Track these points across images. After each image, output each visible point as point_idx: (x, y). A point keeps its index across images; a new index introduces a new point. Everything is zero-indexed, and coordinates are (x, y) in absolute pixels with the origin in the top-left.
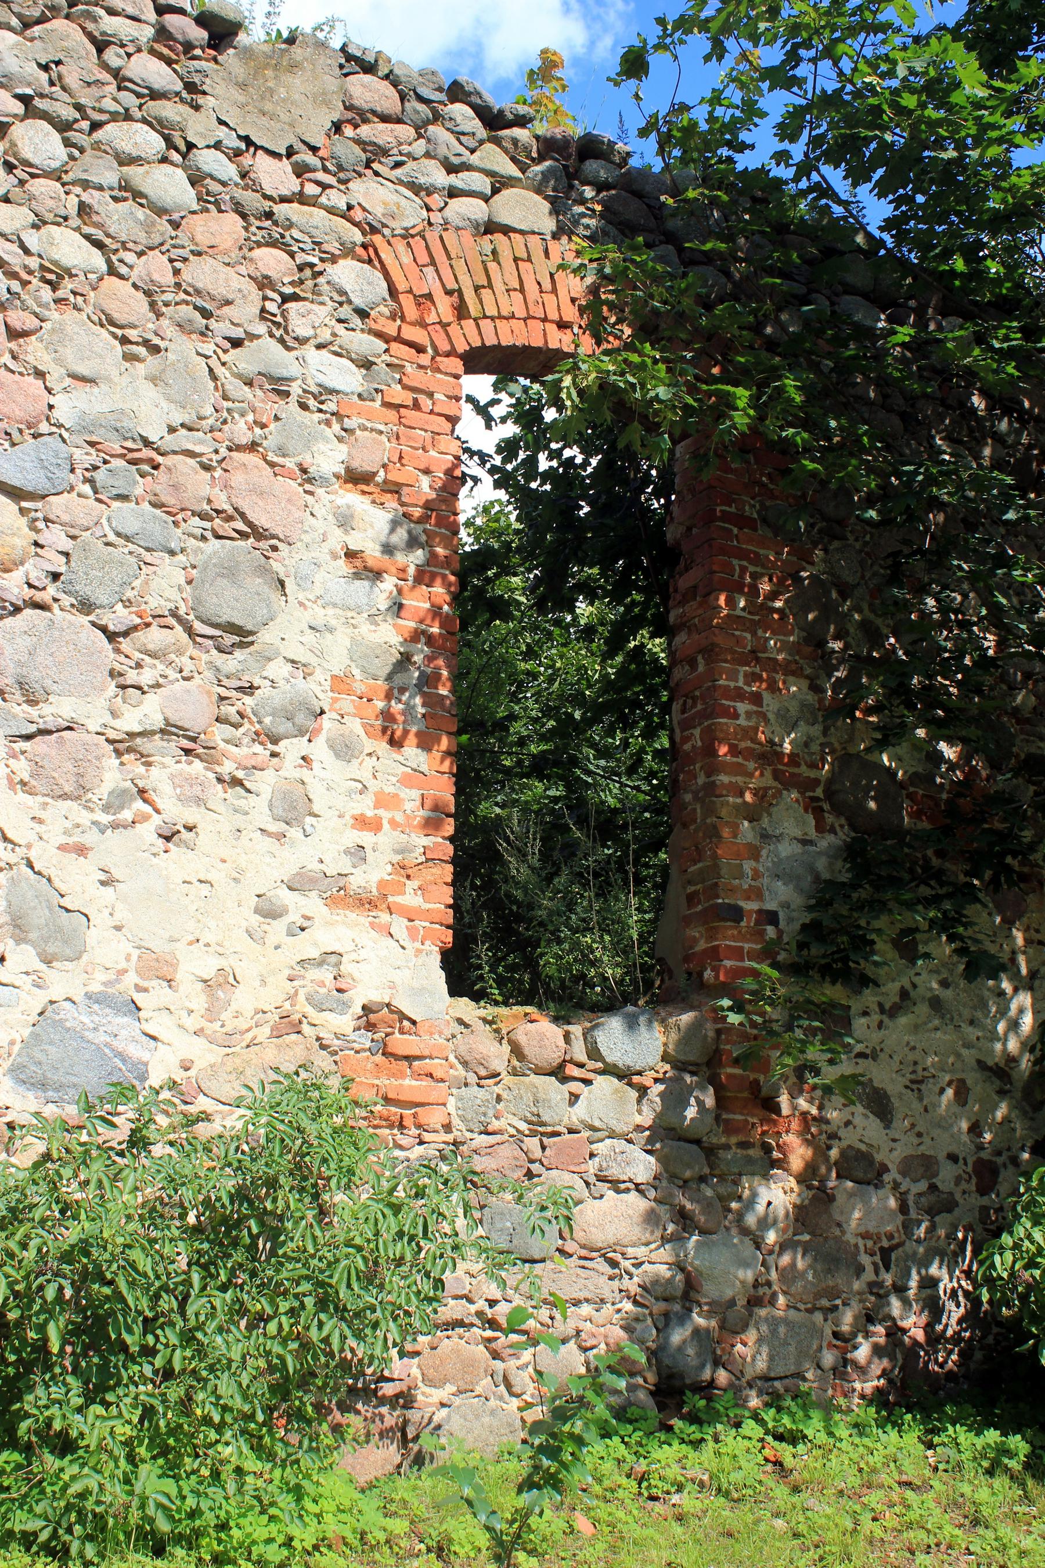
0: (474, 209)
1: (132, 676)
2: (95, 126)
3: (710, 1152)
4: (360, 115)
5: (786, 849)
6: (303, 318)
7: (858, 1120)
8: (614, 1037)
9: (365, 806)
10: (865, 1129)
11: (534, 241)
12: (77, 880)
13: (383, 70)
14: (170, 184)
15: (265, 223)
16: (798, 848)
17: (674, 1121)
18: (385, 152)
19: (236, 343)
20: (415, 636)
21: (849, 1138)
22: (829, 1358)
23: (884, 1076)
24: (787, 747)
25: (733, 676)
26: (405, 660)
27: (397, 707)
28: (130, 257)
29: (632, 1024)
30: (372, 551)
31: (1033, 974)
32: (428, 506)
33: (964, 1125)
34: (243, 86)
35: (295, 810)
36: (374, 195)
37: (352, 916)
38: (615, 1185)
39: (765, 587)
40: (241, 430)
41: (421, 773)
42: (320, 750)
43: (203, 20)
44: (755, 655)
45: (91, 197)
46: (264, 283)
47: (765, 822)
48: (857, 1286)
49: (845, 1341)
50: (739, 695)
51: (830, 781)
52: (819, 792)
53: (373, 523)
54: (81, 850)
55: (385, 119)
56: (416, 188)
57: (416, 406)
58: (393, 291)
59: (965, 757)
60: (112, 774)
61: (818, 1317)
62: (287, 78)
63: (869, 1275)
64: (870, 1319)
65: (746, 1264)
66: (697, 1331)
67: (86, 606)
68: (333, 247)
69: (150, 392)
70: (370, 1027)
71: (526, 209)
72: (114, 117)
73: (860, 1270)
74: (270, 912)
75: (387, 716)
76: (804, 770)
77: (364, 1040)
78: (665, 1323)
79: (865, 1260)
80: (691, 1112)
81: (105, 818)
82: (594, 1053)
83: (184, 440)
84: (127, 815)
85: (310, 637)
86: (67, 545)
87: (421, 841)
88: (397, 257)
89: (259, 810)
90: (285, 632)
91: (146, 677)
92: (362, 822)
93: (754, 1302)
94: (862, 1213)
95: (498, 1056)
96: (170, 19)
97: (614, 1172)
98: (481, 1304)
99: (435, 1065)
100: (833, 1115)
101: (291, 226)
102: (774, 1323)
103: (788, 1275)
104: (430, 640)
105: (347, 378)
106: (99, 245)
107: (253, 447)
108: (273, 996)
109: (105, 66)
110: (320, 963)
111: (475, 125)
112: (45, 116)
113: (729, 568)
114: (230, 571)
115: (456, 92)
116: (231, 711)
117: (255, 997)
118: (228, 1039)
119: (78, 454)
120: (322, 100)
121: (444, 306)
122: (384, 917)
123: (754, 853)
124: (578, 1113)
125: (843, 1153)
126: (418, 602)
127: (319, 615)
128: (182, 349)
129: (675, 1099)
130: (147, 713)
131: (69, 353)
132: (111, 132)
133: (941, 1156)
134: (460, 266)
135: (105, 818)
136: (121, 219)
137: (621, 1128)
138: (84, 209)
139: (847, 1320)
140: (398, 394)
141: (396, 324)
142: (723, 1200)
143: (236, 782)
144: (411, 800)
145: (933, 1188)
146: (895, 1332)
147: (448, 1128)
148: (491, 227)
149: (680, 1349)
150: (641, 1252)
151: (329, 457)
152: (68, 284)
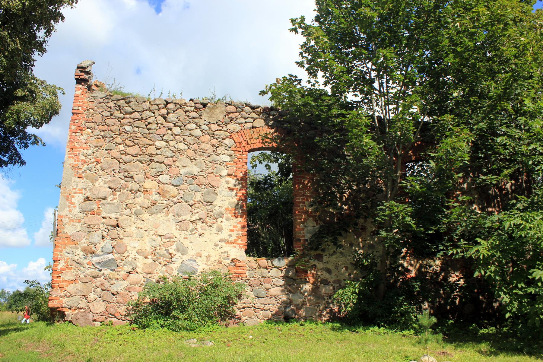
0: (250, 125)
1: (194, 211)
2: (185, 125)
3: (295, 280)
4: (229, 113)
5: (309, 228)
6: (219, 151)
7: (324, 274)
8: (276, 262)
9: (232, 228)
10: (326, 276)
11: (261, 129)
12: (186, 243)
13: (233, 104)
14: (198, 132)
15: (213, 136)
16: (312, 228)
17: (287, 275)
18: (233, 119)
19: (209, 156)
20: (239, 200)
21: (322, 277)
22: (317, 314)
23: (330, 266)
24: (310, 210)
25: (299, 199)
26: (238, 204)
27: (236, 211)
28: (191, 146)
29: (279, 260)
30: (232, 187)
31: (363, 246)
32: (241, 178)
33: (347, 274)
34: (208, 113)
35: (220, 229)
36: (232, 126)
37: (230, 245)
38: (276, 285)
39: (306, 182)
40: (210, 170)
41: (242, 221)
42: (224, 220)
43: (202, 104)
44: (304, 195)
45: (185, 137)
46: (213, 146)
47: (305, 224)
48: (324, 302)
49: (322, 311)
50: (300, 202)
51: (319, 216)
52: (317, 218)
53: (232, 181)
54: (187, 238)
55: (233, 113)
56: (239, 124)
57: (239, 161)
58: (235, 143)
59: (349, 208)
60: (191, 226)
61: (316, 307)
62: (216, 110)
63: (326, 300)
64: (326, 307)
65: (301, 298)
66: (292, 309)
67: (186, 202)
68: (225, 137)
69: (195, 167)
70: (233, 262)
71: (260, 123)
72: (188, 123)
73: (324, 299)
74: (216, 245)
75: (235, 213)
76: (313, 214)
77: (232, 264)
78: (286, 308)
79: (326, 298)
80: (290, 274)
81: (190, 233)
82: (273, 265)
83: (201, 173)
84: (194, 232)
85: (222, 202)
86: (183, 193)
87: (241, 233)
88: (236, 137)
89: (214, 230)
90: (218, 202)
91: (196, 211)
92: (231, 230)
93: (303, 305)
94: (324, 290)
95: (255, 265)
96: (197, 105)
97: (276, 284)
98: (253, 304)
99: (244, 268)
100: (319, 273)
101: (217, 135)
102: (306, 308)
103: (309, 300)
104: (242, 200)
105: (228, 159)
106: (186, 145)
107: (212, 173)
108: (217, 258)
109: (186, 116)
110: (225, 253)
111: (250, 110)
112: (177, 126)
113: (299, 180)
114: (208, 193)
115: (247, 105)
116: (209, 215)
117: (214, 258)
118: (210, 265)
119: (184, 178)
120: (222, 112)
121: (244, 143)
122: (235, 245)
123: (303, 229)
124: (269, 275)
125: (321, 280)
126: (240, 194)
127: (223, 198)
128: (200, 159)
129: (287, 271)
130: (196, 217)
131: (182, 163)
132: (188, 126)
133: (342, 280)
134: (247, 136)
135: (190, 233)
136: (190, 140)
137: (277, 276)
138: (184, 139)
139: (321, 308)
140: (236, 160)
141: (237, 149)
142: (297, 288)
143: (210, 226)
144: (239, 226)
145: (340, 285)
146: (331, 310)
147: (246, 277)
148: (253, 127)
149: (288, 312)
150: (281, 296)
151: (225, 172)
152: (182, 152)
